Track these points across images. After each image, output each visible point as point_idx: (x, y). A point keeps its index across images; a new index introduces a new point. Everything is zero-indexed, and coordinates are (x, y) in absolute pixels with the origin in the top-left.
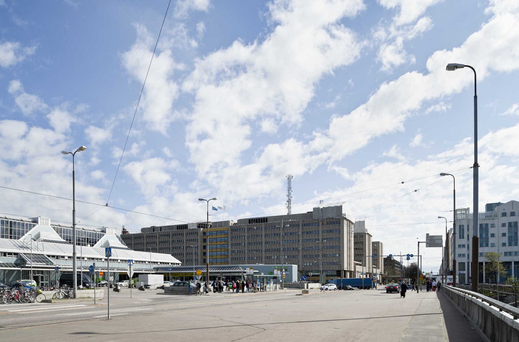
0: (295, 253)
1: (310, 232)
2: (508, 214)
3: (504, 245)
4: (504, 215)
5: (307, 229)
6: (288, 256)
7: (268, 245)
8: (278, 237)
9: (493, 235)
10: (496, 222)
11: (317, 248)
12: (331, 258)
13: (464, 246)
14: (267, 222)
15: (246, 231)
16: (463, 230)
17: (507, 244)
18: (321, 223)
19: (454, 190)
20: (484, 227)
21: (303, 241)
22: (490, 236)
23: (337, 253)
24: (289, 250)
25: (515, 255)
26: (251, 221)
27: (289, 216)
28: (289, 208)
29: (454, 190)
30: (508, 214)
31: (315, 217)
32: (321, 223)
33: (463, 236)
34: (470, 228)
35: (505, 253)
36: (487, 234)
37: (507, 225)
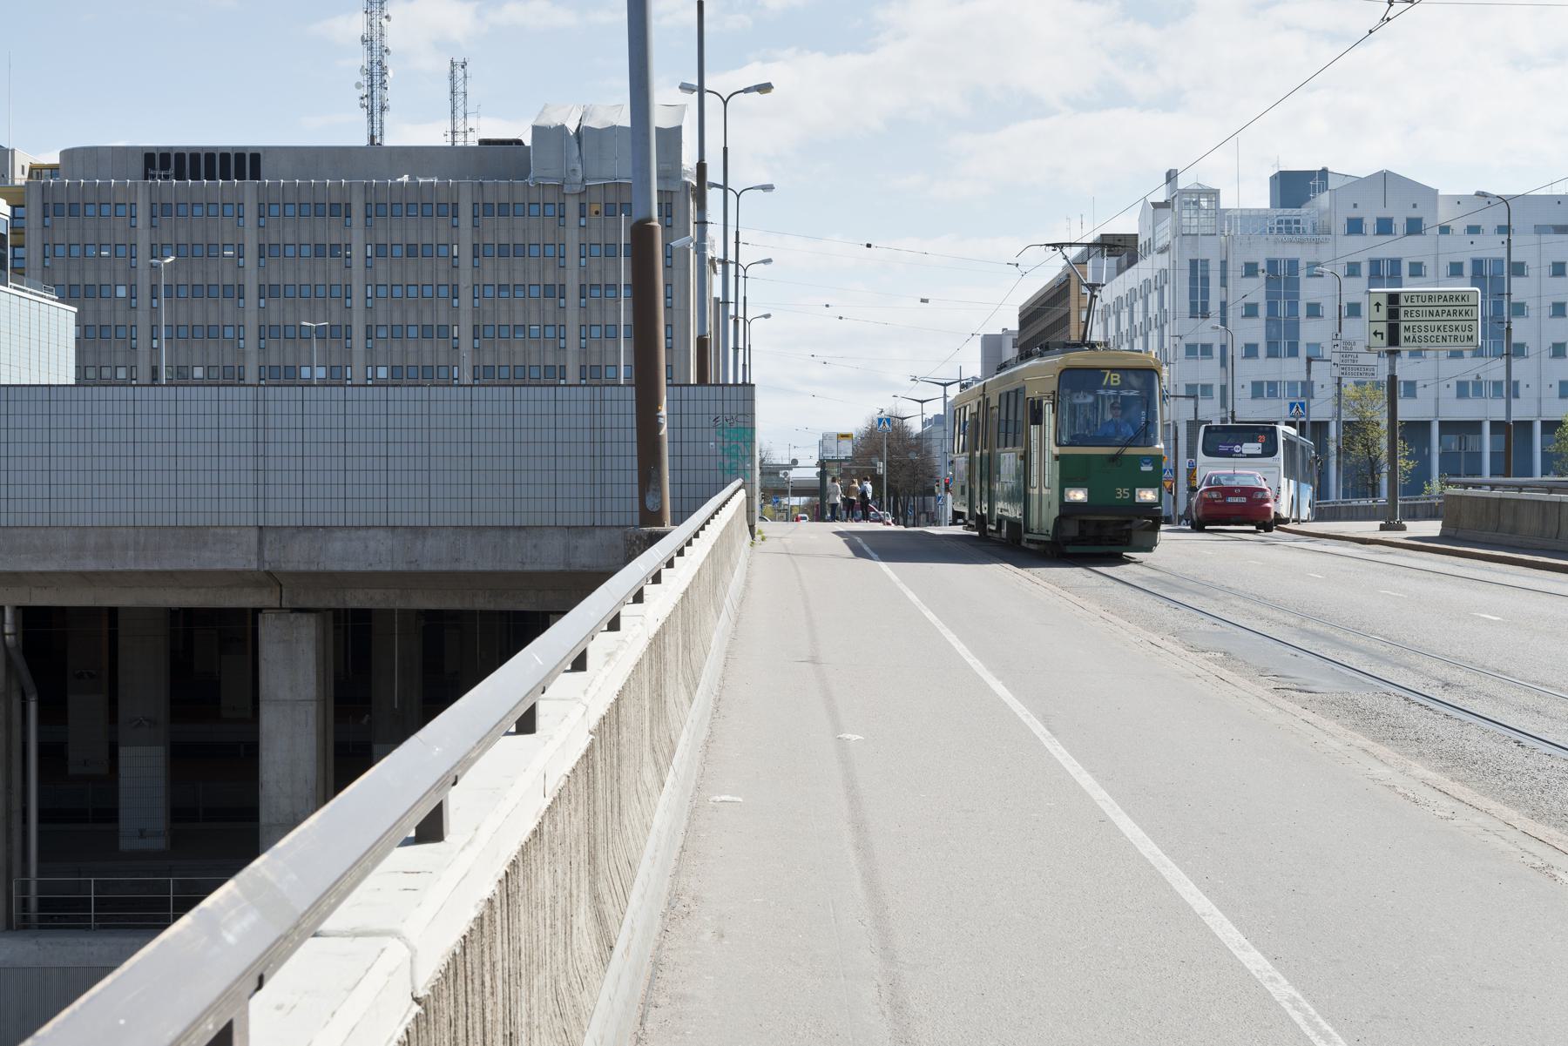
0: (431, 353)
1: (519, 250)
2: (1370, 225)
3: (1251, 351)
4: (1355, 226)
5: (499, 231)
6: (393, 370)
7: (274, 305)
8: (335, 265)
9: (1314, 311)
10: (1324, 253)
11: (550, 332)
12: (412, 346)
13: (1207, 350)
14: (256, 175)
15: (142, 219)
16: (1206, 280)
17: (1262, 350)
18: (572, 207)
19: (725, 150)
20: (1282, 271)
21: (478, 290)
22: (1302, 311)
23: (120, 279)
24: (398, 332)
25: (1272, 385)
26: (159, 162)
27: (453, 148)
28: (374, 107)
29: (725, 150)
30: (1370, 225)
31: (543, 169)
32: (572, 207)
33: (1205, 305)
34: (1218, 274)
35: (1254, 384)
36: (1293, 305)
37: (1365, 270)
